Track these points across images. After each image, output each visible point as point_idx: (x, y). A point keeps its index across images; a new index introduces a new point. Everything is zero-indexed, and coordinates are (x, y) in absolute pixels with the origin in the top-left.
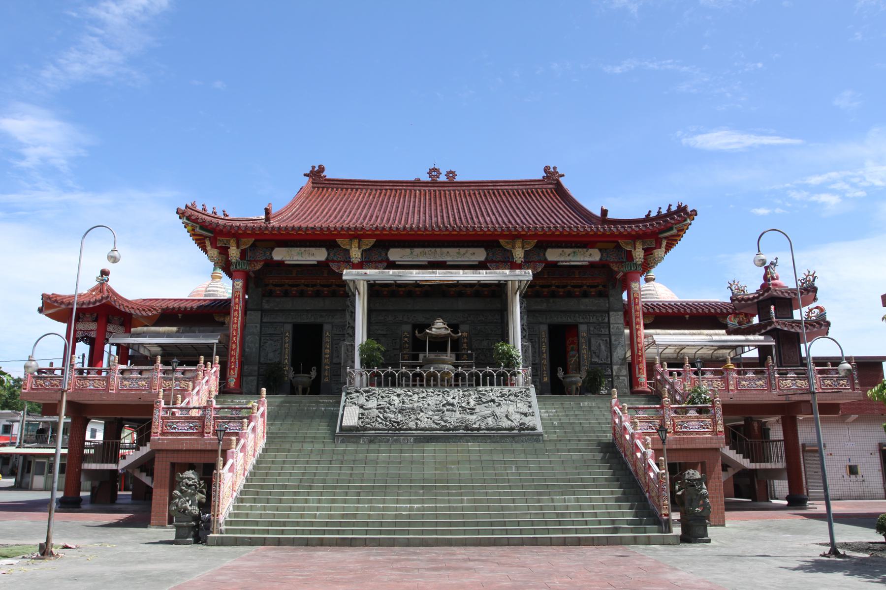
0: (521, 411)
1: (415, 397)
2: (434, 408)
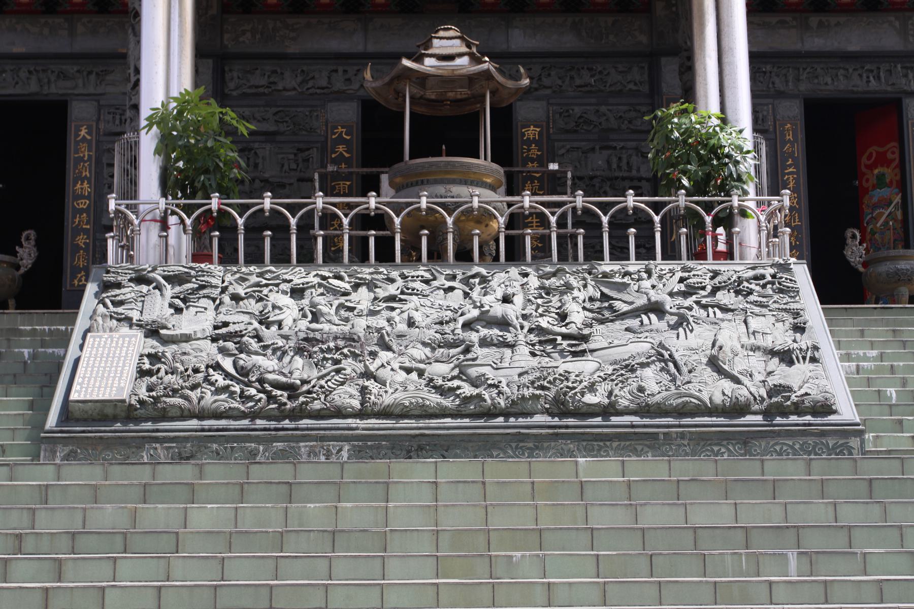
0: (768, 342)
1: (363, 299)
2: (431, 334)
